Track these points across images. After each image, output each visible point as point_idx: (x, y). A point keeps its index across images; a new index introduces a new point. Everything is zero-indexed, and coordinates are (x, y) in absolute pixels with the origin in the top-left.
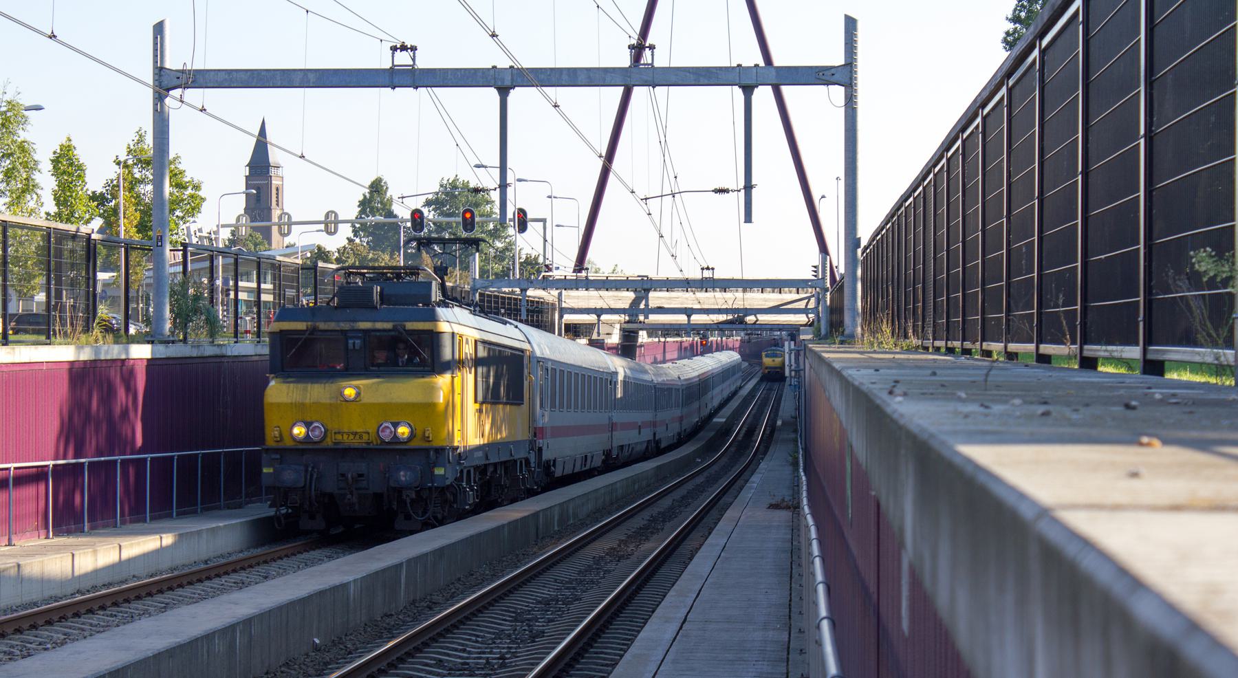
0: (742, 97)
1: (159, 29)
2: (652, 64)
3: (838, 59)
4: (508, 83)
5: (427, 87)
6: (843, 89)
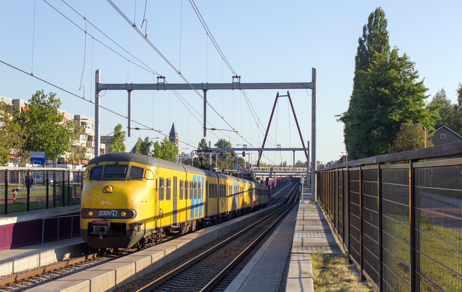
0: (203, 93)
1: (97, 72)
2: (239, 83)
3: (310, 80)
4: (130, 89)
5: (172, 89)
6: (311, 90)
